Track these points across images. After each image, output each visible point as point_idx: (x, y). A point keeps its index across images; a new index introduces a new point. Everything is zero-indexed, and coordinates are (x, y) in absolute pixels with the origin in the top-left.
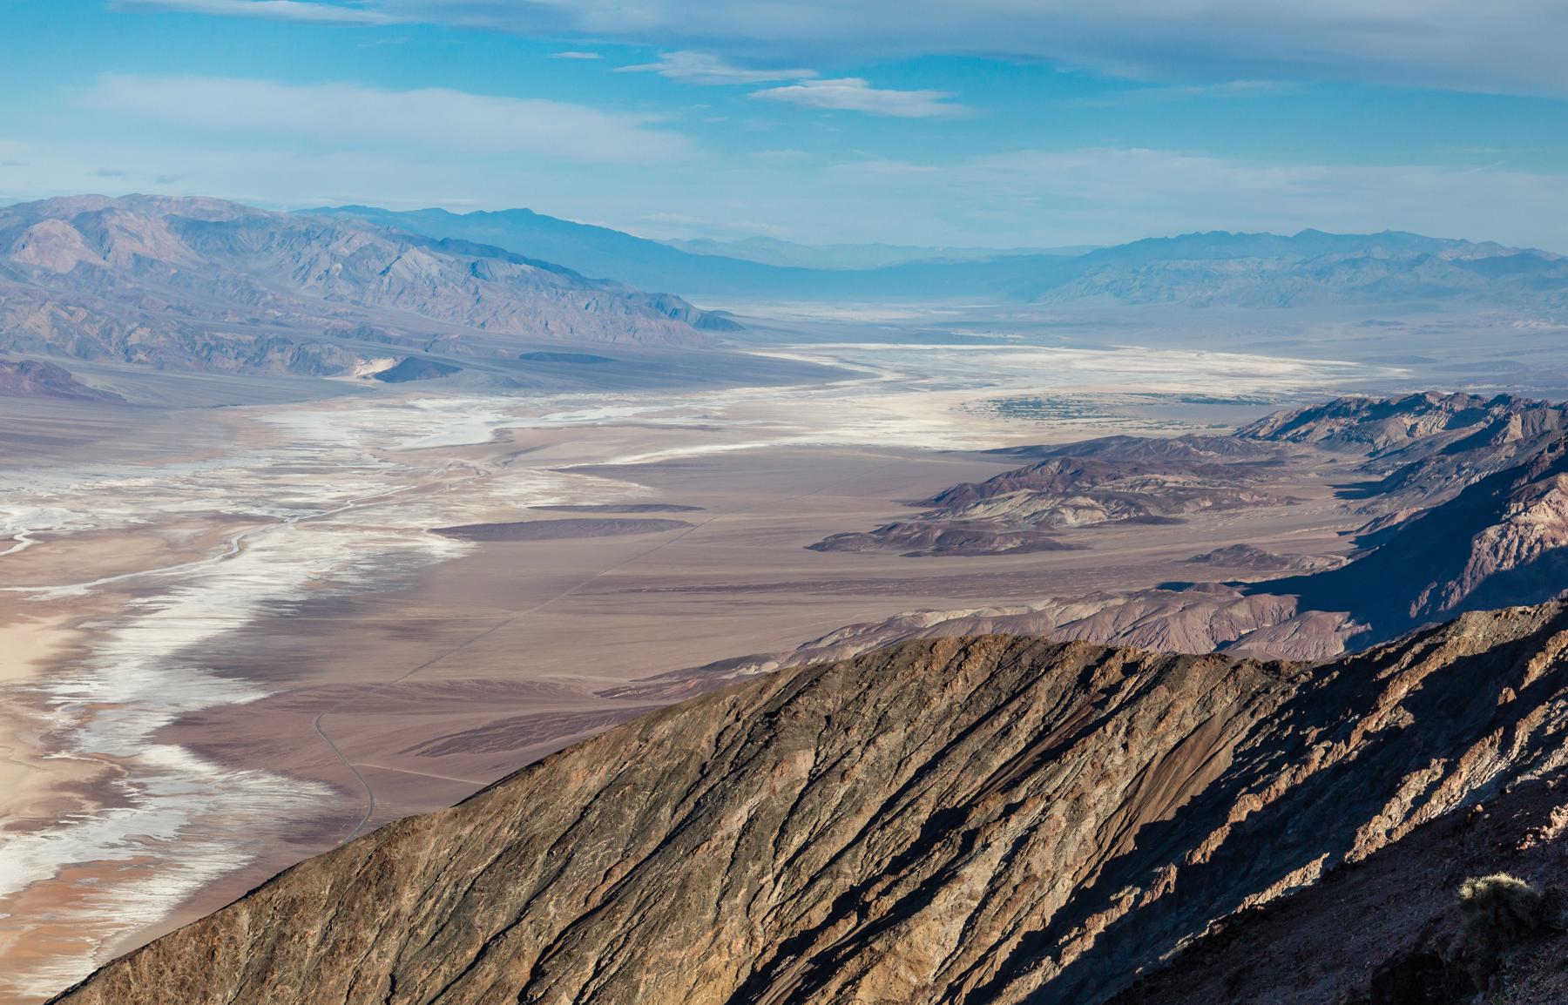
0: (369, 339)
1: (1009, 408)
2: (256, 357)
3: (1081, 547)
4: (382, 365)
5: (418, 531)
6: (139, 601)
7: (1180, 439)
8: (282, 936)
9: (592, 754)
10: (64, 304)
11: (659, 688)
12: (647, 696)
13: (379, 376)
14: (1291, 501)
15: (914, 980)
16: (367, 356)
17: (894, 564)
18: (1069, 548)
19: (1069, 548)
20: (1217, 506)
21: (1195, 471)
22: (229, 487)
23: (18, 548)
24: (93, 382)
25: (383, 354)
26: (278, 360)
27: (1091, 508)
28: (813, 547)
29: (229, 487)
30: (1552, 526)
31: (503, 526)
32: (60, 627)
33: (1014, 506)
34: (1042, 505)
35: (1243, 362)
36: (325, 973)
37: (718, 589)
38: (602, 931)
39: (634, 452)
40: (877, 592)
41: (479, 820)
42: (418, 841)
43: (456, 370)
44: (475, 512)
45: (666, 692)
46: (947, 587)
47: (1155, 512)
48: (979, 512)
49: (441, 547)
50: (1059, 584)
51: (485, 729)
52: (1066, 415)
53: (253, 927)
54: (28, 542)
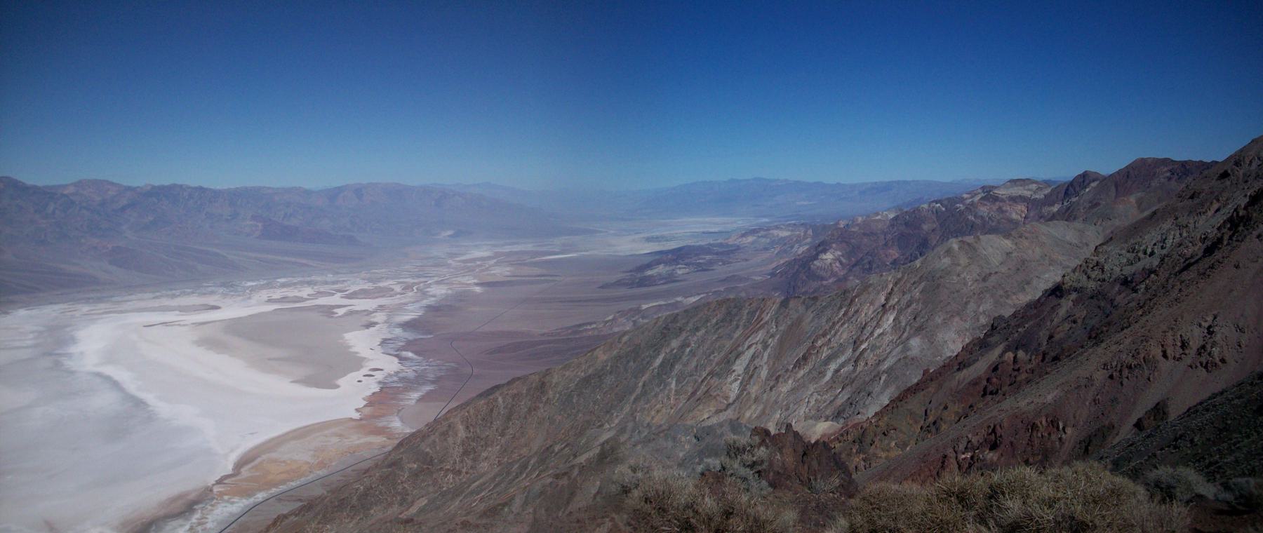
1: (713, 270)
3: (685, 280)
4: (450, 233)
7: (707, 245)
8: (513, 405)
14: (746, 260)
15: (726, 402)
17: (623, 291)
18: (681, 281)
19: (681, 281)
20: (724, 264)
21: (714, 254)
27: (685, 268)
28: (600, 288)
30: (833, 259)
31: (497, 282)
33: (661, 269)
34: (672, 268)
35: (718, 220)
38: (903, 276)
41: (571, 370)
46: (646, 297)
47: (705, 267)
48: (649, 273)
49: (478, 289)
50: (687, 293)
52: (667, 241)
53: (504, 402)
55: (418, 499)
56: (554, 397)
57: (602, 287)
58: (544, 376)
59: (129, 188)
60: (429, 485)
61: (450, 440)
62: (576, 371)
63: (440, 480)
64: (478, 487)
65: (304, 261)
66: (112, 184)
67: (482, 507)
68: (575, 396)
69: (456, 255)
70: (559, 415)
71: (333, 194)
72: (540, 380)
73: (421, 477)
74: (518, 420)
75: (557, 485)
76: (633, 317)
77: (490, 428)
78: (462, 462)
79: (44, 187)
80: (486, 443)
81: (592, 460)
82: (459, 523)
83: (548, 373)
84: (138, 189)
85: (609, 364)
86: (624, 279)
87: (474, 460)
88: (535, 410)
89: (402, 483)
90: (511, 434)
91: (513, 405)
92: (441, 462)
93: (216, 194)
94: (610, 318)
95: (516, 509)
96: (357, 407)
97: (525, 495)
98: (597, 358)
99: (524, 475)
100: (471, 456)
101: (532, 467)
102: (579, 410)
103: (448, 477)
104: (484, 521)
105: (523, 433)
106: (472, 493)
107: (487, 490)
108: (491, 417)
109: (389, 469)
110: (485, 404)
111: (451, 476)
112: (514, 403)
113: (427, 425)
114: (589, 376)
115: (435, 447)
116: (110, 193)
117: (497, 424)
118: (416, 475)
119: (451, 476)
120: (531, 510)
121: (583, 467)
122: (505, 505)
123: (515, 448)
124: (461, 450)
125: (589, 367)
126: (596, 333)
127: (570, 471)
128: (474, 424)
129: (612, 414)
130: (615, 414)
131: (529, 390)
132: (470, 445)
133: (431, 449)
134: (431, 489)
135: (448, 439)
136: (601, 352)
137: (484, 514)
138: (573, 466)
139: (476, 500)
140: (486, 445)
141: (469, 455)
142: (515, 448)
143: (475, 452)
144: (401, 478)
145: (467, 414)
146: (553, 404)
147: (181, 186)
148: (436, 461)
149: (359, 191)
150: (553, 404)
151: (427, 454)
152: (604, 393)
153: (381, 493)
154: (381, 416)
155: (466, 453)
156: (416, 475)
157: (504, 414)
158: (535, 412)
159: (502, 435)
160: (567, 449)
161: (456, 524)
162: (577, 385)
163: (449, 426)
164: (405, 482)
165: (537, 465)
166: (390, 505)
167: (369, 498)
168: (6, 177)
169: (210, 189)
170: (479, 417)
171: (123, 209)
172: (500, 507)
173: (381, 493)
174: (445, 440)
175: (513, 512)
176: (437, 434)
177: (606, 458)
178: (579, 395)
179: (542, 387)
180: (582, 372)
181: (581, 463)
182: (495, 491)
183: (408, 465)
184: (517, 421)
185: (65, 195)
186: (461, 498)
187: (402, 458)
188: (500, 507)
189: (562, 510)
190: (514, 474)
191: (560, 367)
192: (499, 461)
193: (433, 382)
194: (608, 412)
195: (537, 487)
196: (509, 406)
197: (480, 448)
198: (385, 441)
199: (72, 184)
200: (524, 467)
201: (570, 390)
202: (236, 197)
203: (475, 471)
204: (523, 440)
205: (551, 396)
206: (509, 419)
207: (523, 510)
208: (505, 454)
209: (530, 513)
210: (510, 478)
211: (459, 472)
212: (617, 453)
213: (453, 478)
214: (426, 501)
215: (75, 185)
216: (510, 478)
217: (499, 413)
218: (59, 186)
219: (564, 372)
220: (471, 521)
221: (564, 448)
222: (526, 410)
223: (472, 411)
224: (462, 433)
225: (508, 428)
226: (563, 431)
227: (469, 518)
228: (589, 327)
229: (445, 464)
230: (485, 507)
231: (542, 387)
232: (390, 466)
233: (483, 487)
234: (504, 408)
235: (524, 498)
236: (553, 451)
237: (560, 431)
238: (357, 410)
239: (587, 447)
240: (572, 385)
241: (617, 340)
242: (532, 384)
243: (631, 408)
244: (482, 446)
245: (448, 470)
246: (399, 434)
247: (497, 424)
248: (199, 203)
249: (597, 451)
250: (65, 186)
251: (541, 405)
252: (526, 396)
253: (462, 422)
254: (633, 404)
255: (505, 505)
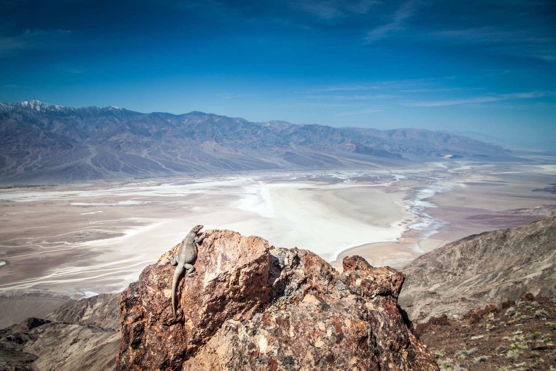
0: (447, 151)
2: (429, 154)
4: (450, 156)
5: (459, 183)
6: (417, 190)
9: (543, 222)
10: (400, 145)
11: (507, 212)
12: (505, 213)
13: (450, 157)
16: (447, 154)
22: (428, 174)
23: (397, 181)
24: (405, 157)
25: (450, 154)
26: (433, 155)
28: (532, 191)
29: (428, 174)
32: (405, 193)
36: (495, 252)
37: (511, 196)
39: (495, 172)
40: (547, 200)
41: (522, 230)
42: (510, 233)
43: (462, 157)
44: (469, 181)
45: (508, 213)
49: (463, 186)
51: (476, 216)
53: (482, 243)
54: (398, 180)
55: (433, 284)
56: (510, 244)
57: (534, 191)
58: (506, 232)
59: (294, 125)
60: (439, 278)
61: (452, 258)
62: (524, 232)
63: (445, 277)
64: (468, 282)
65: (375, 165)
66: (287, 123)
67: (471, 292)
68: (523, 245)
69: (453, 167)
70: (513, 253)
71: (391, 133)
72: (503, 234)
73: (436, 274)
74: (489, 253)
75: (516, 287)
76: (552, 209)
77: (474, 255)
78: (457, 269)
79: (256, 123)
80: (471, 262)
81: (537, 277)
82: (460, 298)
83: (508, 230)
84: (299, 126)
85: (545, 230)
86: (550, 188)
87: (464, 269)
88: (499, 249)
89: (426, 275)
90: (485, 259)
91: (487, 245)
92: (446, 268)
93: (334, 130)
94: (538, 207)
95: (492, 296)
96: (398, 237)
97: (497, 290)
98: (538, 226)
99: (495, 280)
100: (462, 267)
101: (500, 276)
102: (524, 252)
103: (449, 276)
104: (474, 299)
105: (491, 259)
106: (465, 285)
107: (473, 285)
108: (475, 249)
109: (420, 268)
110: (472, 242)
111: (451, 275)
112: (488, 244)
113: (435, 250)
114: (532, 235)
115: (444, 260)
116: (286, 127)
117: (479, 253)
118: (433, 273)
119: (451, 275)
120: (500, 298)
121: (531, 280)
122: (485, 293)
123: (486, 267)
124: (457, 264)
125: (532, 230)
126: (528, 214)
127: (524, 281)
128: (465, 251)
129: (544, 257)
130: (545, 257)
131: (497, 238)
132: (462, 262)
133: (442, 261)
134: (440, 280)
135: (451, 257)
136: (541, 223)
137: (474, 296)
138: (526, 279)
139: (467, 289)
140: (471, 263)
141: (461, 267)
142: (486, 267)
143: (465, 266)
144: (425, 273)
145: (462, 246)
146: (510, 247)
147: (318, 125)
148: (444, 267)
149: (404, 132)
150: (510, 247)
151: (440, 263)
152: (540, 245)
153: (414, 279)
154: (410, 243)
155: (460, 265)
156: (433, 273)
157: (482, 249)
158: (499, 250)
159: (480, 259)
160: (520, 270)
161: (459, 298)
162: (524, 239)
163: (452, 251)
164: (427, 275)
165: (502, 276)
166: (419, 285)
167: (408, 280)
168: (240, 118)
169: (332, 128)
170: (469, 249)
171: (291, 135)
172: (483, 294)
173: (414, 279)
174: (450, 257)
175: (489, 297)
176: (445, 254)
177: (545, 277)
178: (525, 244)
179: (504, 237)
180: (528, 232)
181: (530, 278)
182: (478, 286)
183: (429, 267)
184: (488, 253)
185: (266, 127)
186: (458, 286)
187: (426, 264)
188: (483, 294)
189: (517, 300)
190: (489, 279)
191: (515, 228)
192: (477, 272)
193: (437, 230)
194: (541, 255)
195: (504, 287)
196: (485, 245)
197: (467, 264)
198: (410, 255)
199: (268, 122)
200: (495, 276)
201: (520, 241)
202: (344, 133)
203: (464, 275)
204: (491, 263)
205: (509, 243)
206: (485, 251)
207: (495, 297)
208: (481, 269)
209: (499, 299)
210: (487, 280)
211: (455, 275)
212: (552, 276)
213: (452, 277)
214: (439, 286)
215: (271, 122)
216: (487, 280)
217: (479, 248)
218: (263, 123)
219: (517, 232)
220: (467, 298)
221: (519, 269)
222: (494, 248)
223: (465, 245)
224: (459, 256)
225: (483, 256)
226: (514, 262)
227: (465, 296)
228: (524, 211)
229: (448, 269)
230: (473, 293)
231: (504, 237)
232: (420, 266)
233: (471, 283)
234: (482, 246)
235: (496, 291)
236: (512, 270)
237: (512, 261)
238: (397, 239)
239: (534, 271)
240: (521, 239)
241: (552, 219)
242: (499, 235)
243: (554, 256)
244: (469, 263)
245: (449, 273)
246: (418, 253)
247: (479, 253)
248: (326, 133)
249: (540, 273)
250: (266, 123)
251: (503, 247)
252: (495, 241)
253: (459, 250)
254: (555, 254)
255: (485, 293)
